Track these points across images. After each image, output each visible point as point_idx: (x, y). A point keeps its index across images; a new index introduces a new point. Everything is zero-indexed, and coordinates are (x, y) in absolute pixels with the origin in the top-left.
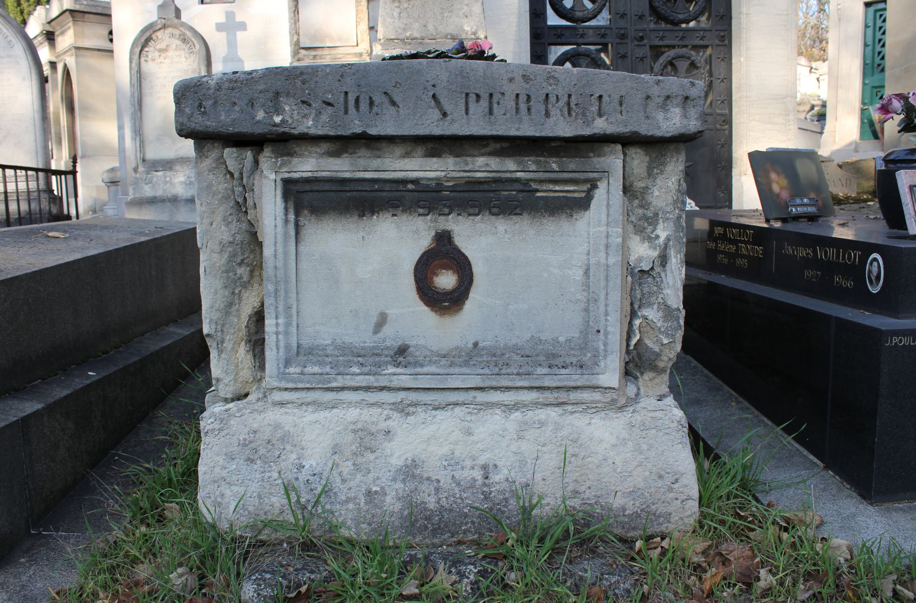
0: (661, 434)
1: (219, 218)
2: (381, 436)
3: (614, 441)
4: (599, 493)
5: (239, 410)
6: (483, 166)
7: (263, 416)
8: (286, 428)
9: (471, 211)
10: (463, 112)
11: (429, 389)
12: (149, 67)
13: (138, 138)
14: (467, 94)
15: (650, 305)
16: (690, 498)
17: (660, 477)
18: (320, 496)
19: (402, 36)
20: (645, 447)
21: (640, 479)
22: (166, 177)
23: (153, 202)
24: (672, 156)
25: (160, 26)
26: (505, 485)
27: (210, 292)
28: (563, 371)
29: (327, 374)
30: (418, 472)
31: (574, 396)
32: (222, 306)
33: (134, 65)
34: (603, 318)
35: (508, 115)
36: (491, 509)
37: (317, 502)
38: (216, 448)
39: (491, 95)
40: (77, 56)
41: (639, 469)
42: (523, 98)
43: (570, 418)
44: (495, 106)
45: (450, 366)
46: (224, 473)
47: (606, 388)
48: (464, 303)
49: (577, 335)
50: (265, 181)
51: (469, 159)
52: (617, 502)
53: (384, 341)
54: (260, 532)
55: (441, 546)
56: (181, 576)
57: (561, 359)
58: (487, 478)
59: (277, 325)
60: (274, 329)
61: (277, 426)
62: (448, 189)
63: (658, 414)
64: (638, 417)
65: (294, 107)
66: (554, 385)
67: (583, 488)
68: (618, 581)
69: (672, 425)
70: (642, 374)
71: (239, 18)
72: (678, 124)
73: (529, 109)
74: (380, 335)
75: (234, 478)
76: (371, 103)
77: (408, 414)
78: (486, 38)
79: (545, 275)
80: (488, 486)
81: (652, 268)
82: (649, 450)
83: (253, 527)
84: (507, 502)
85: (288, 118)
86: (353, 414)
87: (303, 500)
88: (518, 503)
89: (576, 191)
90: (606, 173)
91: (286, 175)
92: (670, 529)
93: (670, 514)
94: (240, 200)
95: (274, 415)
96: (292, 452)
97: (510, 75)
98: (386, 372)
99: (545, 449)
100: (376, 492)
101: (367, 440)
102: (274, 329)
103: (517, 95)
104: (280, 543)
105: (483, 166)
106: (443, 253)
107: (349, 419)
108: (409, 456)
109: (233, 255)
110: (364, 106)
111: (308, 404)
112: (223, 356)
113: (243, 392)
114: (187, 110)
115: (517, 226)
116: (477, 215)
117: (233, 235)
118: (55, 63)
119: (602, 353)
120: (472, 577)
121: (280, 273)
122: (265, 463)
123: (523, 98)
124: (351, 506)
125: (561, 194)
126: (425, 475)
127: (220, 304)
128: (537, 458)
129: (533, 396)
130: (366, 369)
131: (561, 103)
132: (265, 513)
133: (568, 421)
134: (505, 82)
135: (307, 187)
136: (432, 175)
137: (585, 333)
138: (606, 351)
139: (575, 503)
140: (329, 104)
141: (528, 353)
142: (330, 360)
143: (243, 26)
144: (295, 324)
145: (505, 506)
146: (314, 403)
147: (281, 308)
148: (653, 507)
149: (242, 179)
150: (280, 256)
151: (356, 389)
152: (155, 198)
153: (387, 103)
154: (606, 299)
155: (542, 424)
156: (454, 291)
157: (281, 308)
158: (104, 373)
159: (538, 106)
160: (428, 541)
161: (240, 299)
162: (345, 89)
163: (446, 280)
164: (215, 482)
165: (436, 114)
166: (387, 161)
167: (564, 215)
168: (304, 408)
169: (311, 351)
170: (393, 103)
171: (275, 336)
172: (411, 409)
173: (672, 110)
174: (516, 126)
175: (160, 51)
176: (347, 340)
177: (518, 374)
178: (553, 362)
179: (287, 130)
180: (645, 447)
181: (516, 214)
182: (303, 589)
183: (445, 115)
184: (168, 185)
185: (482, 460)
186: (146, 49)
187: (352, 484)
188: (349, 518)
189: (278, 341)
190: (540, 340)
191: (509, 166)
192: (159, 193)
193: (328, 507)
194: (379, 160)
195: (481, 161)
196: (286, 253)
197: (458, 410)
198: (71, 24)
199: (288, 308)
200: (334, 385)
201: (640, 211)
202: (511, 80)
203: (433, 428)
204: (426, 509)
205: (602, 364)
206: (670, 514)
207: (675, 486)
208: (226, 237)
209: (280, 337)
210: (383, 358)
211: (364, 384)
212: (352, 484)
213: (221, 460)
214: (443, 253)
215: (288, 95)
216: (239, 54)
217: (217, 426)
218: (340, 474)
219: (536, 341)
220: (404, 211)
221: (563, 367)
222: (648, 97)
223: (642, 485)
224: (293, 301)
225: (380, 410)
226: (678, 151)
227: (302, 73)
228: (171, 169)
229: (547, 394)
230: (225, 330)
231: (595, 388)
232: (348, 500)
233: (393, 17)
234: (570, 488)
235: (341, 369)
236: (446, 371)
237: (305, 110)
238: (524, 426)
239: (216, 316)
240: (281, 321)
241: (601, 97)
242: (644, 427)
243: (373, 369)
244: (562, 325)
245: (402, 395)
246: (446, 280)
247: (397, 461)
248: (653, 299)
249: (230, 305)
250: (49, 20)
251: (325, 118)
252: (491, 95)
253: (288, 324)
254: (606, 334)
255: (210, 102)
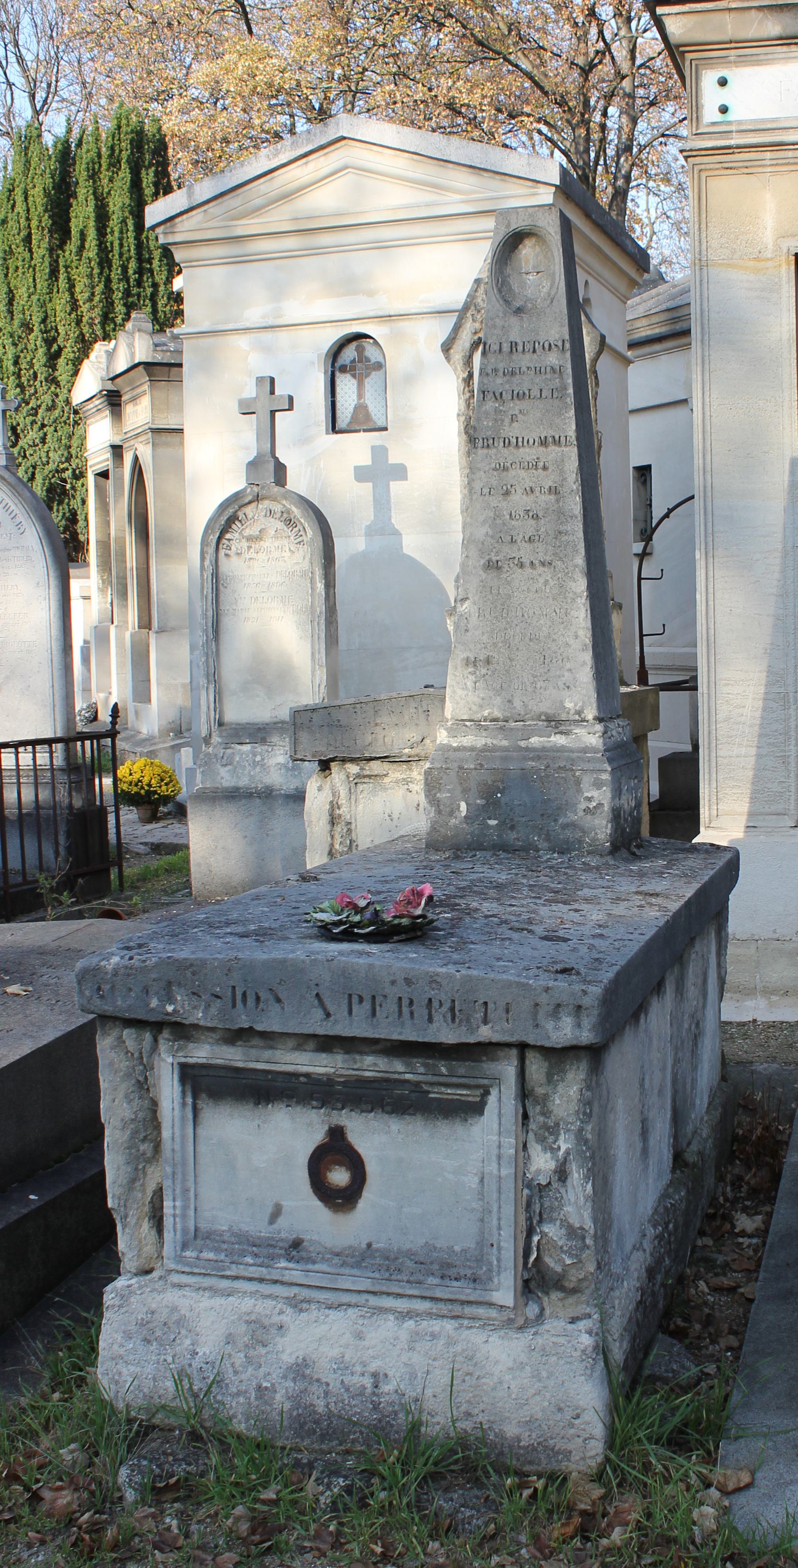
0: (562, 1362)
1: (121, 1095)
2: (273, 1331)
3: (510, 1364)
4: (492, 1418)
5: (140, 1288)
6: (372, 1066)
7: (161, 1296)
8: (183, 1312)
9: (364, 1107)
10: (346, 1013)
11: (322, 1288)
12: (231, 566)
13: (212, 687)
14: (350, 996)
15: (552, 1220)
16: (592, 1437)
17: (560, 1410)
18: (210, 1386)
19: (478, 716)
20: (544, 1374)
21: (537, 1409)
22: (255, 755)
23: (233, 797)
24: (572, 1064)
25: (250, 498)
26: (395, 1397)
27: (114, 1166)
28: (455, 1284)
29: (222, 1261)
30: (308, 1372)
31: (468, 1310)
32: (125, 1182)
33: (207, 563)
34: (495, 1231)
35: (390, 1019)
36: (380, 1421)
37: (208, 1392)
38: (115, 1325)
39: (374, 997)
40: (154, 445)
41: (538, 1398)
42: (405, 1002)
43: (466, 1333)
44: (378, 1008)
45: (342, 1266)
46: (122, 1351)
47: (502, 1307)
48: (357, 1202)
49: (473, 1246)
50: (162, 1064)
51: (358, 1057)
52: (511, 1430)
53: (279, 1233)
54: (153, 1416)
55: (330, 1453)
56: (72, 1452)
57: (455, 1270)
58: (376, 1387)
59: (174, 1207)
60: (171, 1211)
61: (174, 1309)
62: (339, 1083)
63: (562, 1340)
64: (540, 1340)
65: (185, 998)
66: (446, 1297)
67: (476, 1411)
68: (472, 1516)
69: (575, 1354)
70: (547, 1293)
71: (393, 459)
72: (569, 1035)
73: (412, 1013)
74: (275, 1226)
75: (131, 1357)
76: (258, 999)
77: (301, 1310)
79: (440, 1180)
80: (377, 1395)
81: (550, 1183)
82: (548, 1377)
83: (147, 1410)
84: (396, 1415)
85: (179, 1008)
86: (247, 1304)
87: (195, 1388)
88: (407, 1417)
89: (471, 1096)
90: (497, 1080)
91: (183, 1060)
92: (570, 1469)
93: (570, 1452)
94: (141, 1079)
95: (172, 1297)
96: (186, 1337)
97: (392, 978)
98: (278, 1265)
99: (436, 1364)
100: (266, 1388)
101: (260, 1332)
102: (171, 1211)
103: (400, 999)
104: (171, 1430)
105: (372, 1066)
106: (335, 1149)
107: (244, 1309)
108: (301, 1354)
109: (135, 1132)
110: (251, 1001)
111: (205, 1289)
112: (127, 1230)
113: (147, 1267)
114: (87, 993)
115: (410, 1127)
116: (371, 1111)
117: (135, 1113)
118: (121, 447)
119: (495, 1269)
120: (336, 1490)
121: (178, 1156)
122: (161, 1345)
123: (405, 1002)
124: (242, 1399)
125: (455, 1097)
126: (316, 1377)
127: (123, 1180)
128: (428, 1372)
129: (425, 1306)
130: (259, 1261)
131: (445, 1008)
132: (160, 1397)
133: (463, 1336)
134: (387, 984)
135: (204, 1073)
136: (321, 1070)
137: (480, 1244)
138: (499, 1267)
139: (465, 1425)
140: (218, 997)
141: (422, 1259)
142: (225, 1246)
143: (400, 472)
144: (192, 1207)
145: (394, 1419)
146: (210, 1288)
147: (178, 1191)
148: (551, 1442)
149: (142, 1058)
150: (178, 1139)
151: (250, 1279)
152: (237, 789)
153: (272, 1000)
154: (499, 1212)
155: (434, 1336)
156: (346, 1189)
157: (178, 1191)
158: (49, 1196)
159: (421, 1011)
160: (316, 1446)
161: (145, 1174)
162: (232, 983)
163: (339, 1177)
164: (113, 1359)
165: (319, 1014)
166: (278, 1053)
167: (458, 1120)
168: (201, 1292)
169: (209, 1236)
170: (278, 1000)
171: (172, 1219)
172: (305, 1306)
173: (564, 1019)
174: (399, 1030)
175: (250, 539)
176: (245, 1228)
177: (408, 1282)
178: (446, 1273)
179: (178, 1019)
180: (544, 1374)
181: (410, 1114)
182: (173, 1481)
183: (328, 1015)
184: (258, 769)
185: (373, 1367)
186: (228, 536)
187: (243, 1377)
188: (238, 1412)
189: (175, 1223)
190: (435, 1248)
191: (398, 1067)
192: (244, 782)
193: (219, 1397)
194: (270, 1052)
195: (369, 1060)
196: (183, 1137)
197: (350, 1311)
198: (146, 387)
199: (186, 1191)
200: (228, 1273)
201: (541, 1119)
202: (393, 983)
203: (325, 1327)
204: (315, 1412)
205: (496, 1280)
206: (570, 1452)
207: (577, 1422)
208: (128, 1114)
209: (178, 1220)
210: (277, 1251)
211: (256, 1275)
212: (243, 1377)
213: (119, 1337)
214: (335, 1149)
215: (179, 985)
216: (393, 521)
217: (117, 1303)
218: (233, 1365)
219: (430, 1247)
220: (298, 1102)
221: (456, 1279)
222: (537, 1005)
223: (540, 1415)
224: (191, 1184)
225: (274, 1302)
226: (578, 1059)
227: (192, 965)
228: (263, 741)
229: (441, 1305)
230: (128, 1204)
231: (490, 1304)
232: (239, 1394)
233: (465, 688)
234: (463, 1408)
235: (236, 1258)
236: (337, 1271)
237: (195, 1000)
238: (415, 1337)
239: (118, 1191)
240: (178, 1204)
241: (486, 1003)
242: (544, 1352)
243: (266, 1261)
244: (456, 1234)
245: (295, 1290)
246: (339, 1177)
247: (288, 1358)
248: (555, 1215)
249: (133, 1181)
250: (111, 375)
251: (213, 1011)
252: (374, 997)
253: (185, 1208)
254: (499, 1249)
255: (108, 987)
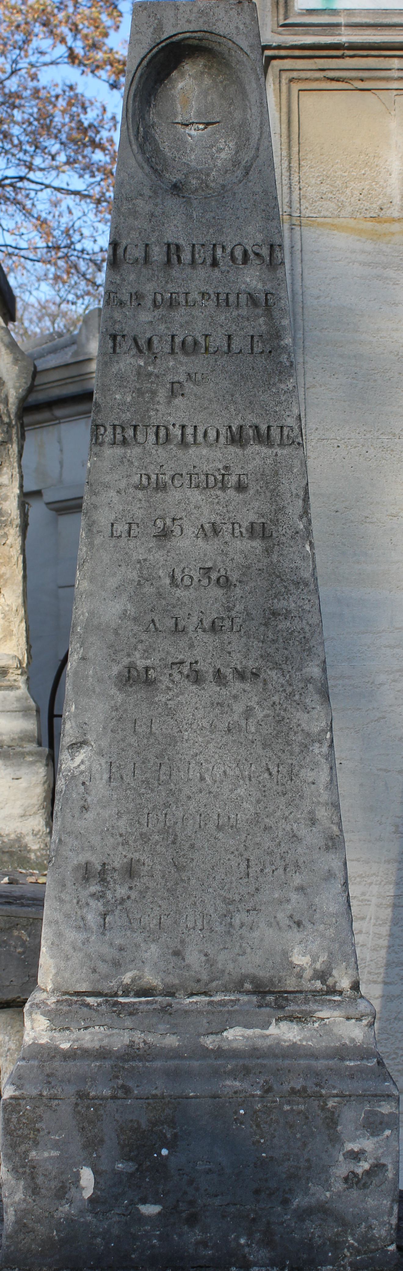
22: (295, 1134)
78: (356, 986)
233: (82, 926)
